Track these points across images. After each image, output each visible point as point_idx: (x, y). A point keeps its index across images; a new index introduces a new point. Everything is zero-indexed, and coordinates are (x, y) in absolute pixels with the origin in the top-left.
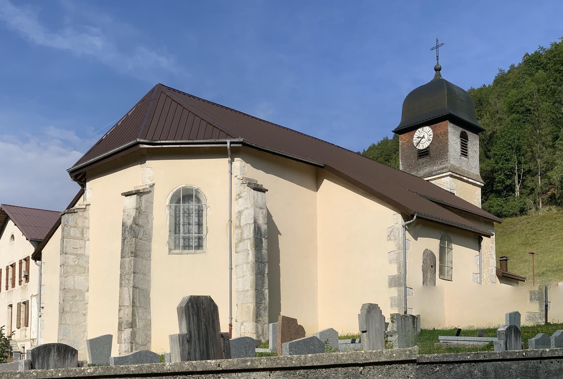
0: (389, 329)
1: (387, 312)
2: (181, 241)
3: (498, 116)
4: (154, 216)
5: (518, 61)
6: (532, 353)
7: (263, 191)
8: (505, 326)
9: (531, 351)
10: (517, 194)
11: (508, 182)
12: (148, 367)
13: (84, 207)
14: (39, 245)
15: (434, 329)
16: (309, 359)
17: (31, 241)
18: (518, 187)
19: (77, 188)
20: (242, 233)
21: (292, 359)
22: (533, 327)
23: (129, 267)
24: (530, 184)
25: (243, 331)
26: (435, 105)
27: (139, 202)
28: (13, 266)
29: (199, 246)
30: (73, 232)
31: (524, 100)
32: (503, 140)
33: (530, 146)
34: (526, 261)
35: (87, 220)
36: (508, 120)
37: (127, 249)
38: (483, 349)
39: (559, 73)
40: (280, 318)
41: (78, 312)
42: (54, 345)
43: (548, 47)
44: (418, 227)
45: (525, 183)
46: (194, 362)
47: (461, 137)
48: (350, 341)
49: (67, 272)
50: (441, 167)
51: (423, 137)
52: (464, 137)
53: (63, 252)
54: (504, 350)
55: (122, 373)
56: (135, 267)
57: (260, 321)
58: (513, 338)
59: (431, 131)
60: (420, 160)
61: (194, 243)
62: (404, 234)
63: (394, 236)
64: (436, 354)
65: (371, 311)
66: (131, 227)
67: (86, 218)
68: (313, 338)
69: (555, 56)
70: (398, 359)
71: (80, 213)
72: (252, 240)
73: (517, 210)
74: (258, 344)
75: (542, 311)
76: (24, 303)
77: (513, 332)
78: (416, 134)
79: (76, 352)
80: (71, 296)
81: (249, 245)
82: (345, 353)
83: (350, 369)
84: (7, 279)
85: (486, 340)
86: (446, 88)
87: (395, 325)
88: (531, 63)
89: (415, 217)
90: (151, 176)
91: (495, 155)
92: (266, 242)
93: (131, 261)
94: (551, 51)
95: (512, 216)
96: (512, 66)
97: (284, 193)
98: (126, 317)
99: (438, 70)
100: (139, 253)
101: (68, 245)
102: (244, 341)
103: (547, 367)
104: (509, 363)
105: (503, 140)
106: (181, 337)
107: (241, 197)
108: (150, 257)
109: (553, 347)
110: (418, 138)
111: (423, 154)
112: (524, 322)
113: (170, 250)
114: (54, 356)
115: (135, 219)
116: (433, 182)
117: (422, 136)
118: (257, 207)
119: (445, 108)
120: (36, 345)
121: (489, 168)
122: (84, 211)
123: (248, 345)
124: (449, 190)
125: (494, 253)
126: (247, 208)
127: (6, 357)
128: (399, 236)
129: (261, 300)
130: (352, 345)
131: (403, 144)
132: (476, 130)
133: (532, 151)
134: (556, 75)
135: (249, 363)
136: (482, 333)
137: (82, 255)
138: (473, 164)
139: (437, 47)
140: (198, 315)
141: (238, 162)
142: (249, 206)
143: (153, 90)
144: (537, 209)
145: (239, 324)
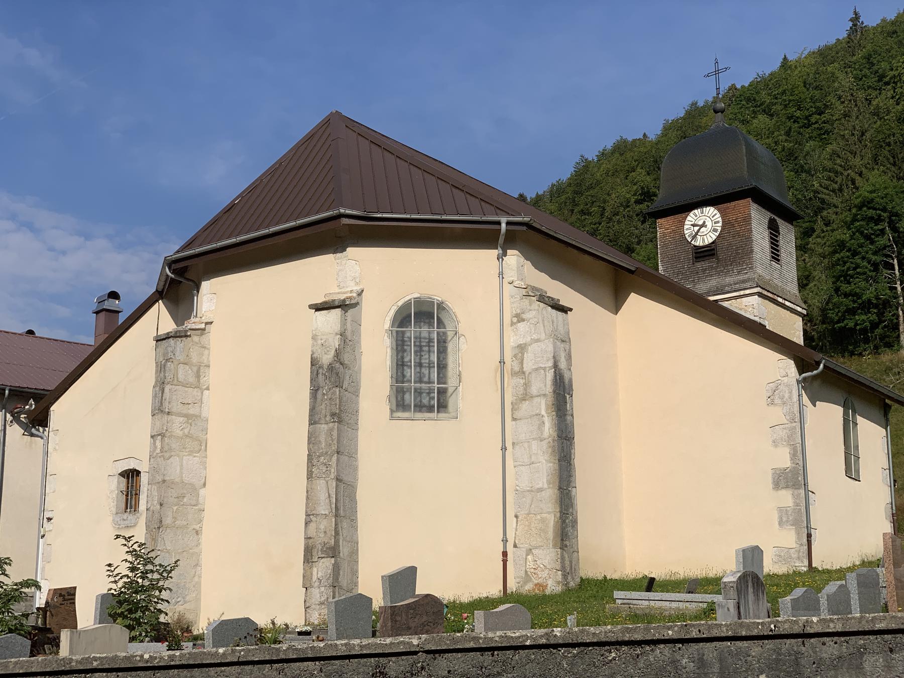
6: (786, 626)
7: (564, 310)
8: (735, 573)
9: (785, 622)
13: (203, 326)
15: (605, 577)
20: (527, 385)
22: (786, 576)
27: (344, 322)
29: (442, 406)
35: (206, 352)
37: (323, 408)
38: (697, 618)
39: (794, 122)
41: (186, 527)
47: (769, 228)
49: (170, 449)
50: (741, 277)
51: (704, 225)
52: (773, 228)
54: (736, 619)
57: (566, 546)
58: (751, 597)
59: (718, 215)
63: (782, 398)
64: (609, 627)
66: (331, 368)
67: (205, 348)
69: (784, 92)
71: (196, 338)
72: (550, 398)
75: (802, 545)
77: (750, 584)
78: (689, 218)
80: (175, 495)
81: (543, 407)
85: (703, 598)
86: (743, 142)
88: (744, 102)
89: (822, 366)
90: (357, 275)
93: (331, 430)
98: (322, 535)
101: (174, 397)
103: (815, 652)
104: (745, 644)
107: (523, 320)
109: (825, 615)
110: (694, 225)
111: (705, 253)
112: (770, 566)
113: (392, 411)
115: (338, 353)
116: (725, 304)
117: (700, 223)
122: (202, 335)
124: (757, 319)
126: (538, 341)
128: (790, 398)
131: (664, 235)
132: (790, 217)
134: (789, 124)
136: (693, 585)
137: (197, 416)
138: (786, 276)
139: (717, 72)
141: (513, 258)
142: (543, 336)
145: (521, 552)
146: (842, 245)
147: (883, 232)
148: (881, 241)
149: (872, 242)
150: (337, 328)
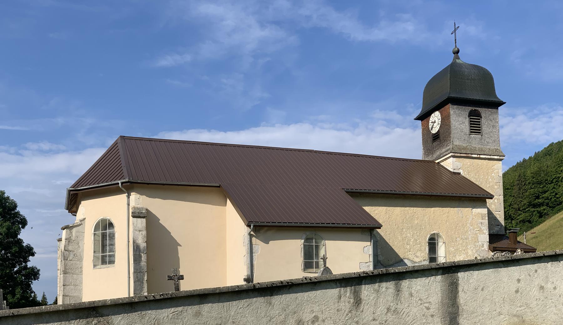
4: (85, 242)
99: (457, 52)
108: (81, 272)
110: (432, 122)
113: (95, 266)
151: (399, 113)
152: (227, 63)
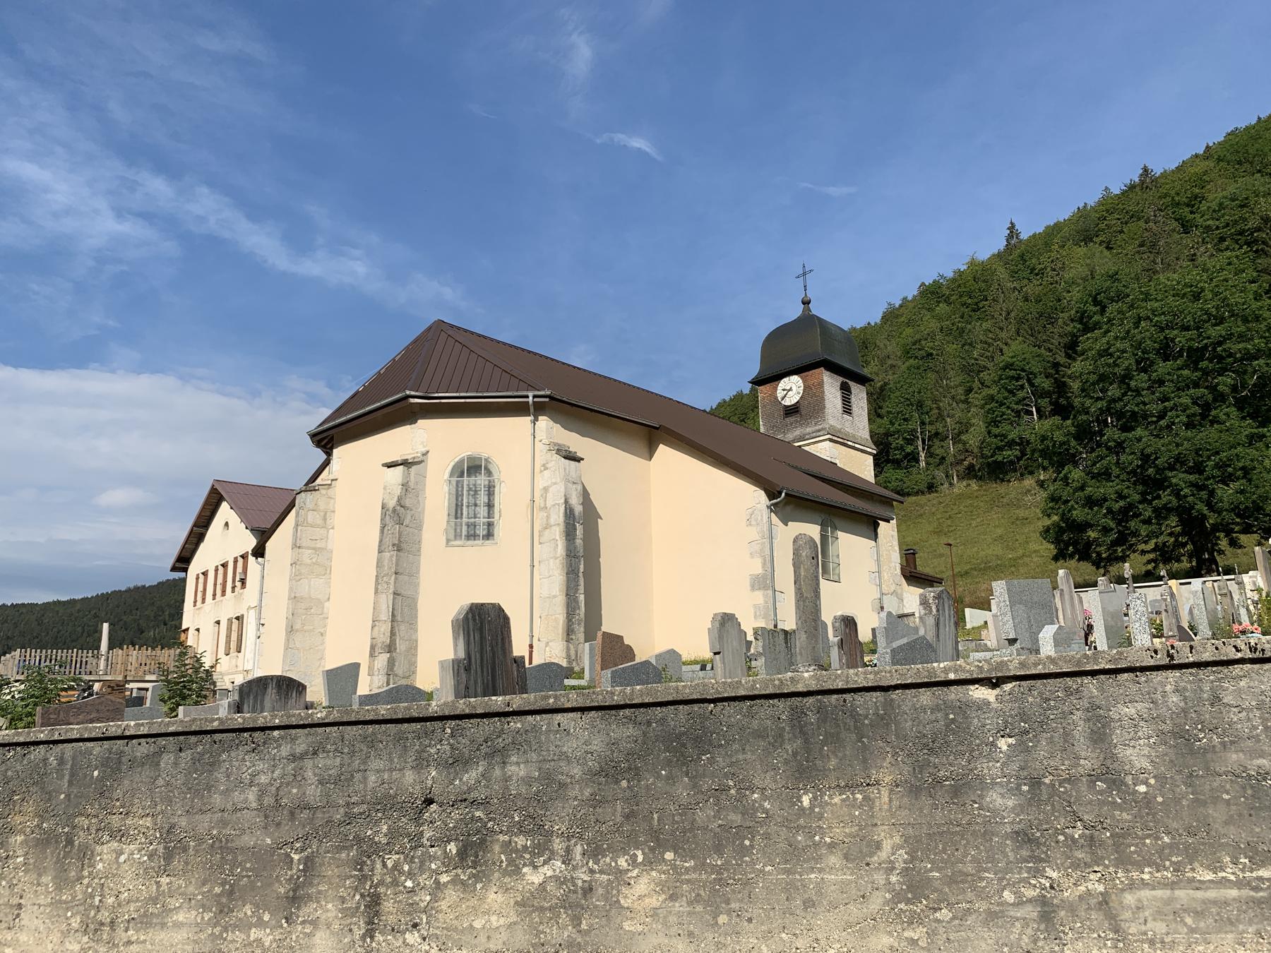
0: (752, 651)
1: (749, 624)
2: (464, 528)
3: (890, 362)
5: (912, 292)
7: (578, 460)
10: (923, 464)
11: (909, 449)
12: (405, 708)
14: (264, 536)
16: (638, 692)
17: (252, 530)
18: (922, 455)
19: (320, 456)
20: (548, 517)
21: (613, 693)
23: (388, 566)
24: (939, 451)
25: (548, 654)
26: (804, 347)
27: (407, 476)
28: (224, 565)
29: (489, 535)
30: (311, 517)
31: (923, 342)
32: (898, 394)
33: (935, 401)
34: (941, 555)
36: (904, 367)
40: (599, 634)
42: (272, 678)
43: (950, 274)
44: (788, 508)
45: (932, 450)
46: (472, 700)
48: (698, 667)
50: (817, 428)
51: (790, 389)
52: (845, 389)
53: (296, 546)
55: (368, 718)
56: (397, 565)
60: (787, 420)
61: (481, 531)
62: (770, 517)
65: (726, 622)
66: (394, 510)
68: (647, 663)
70: (763, 692)
71: (323, 492)
73: (923, 486)
74: (569, 673)
76: (237, 618)
79: (304, 687)
82: (434, 707)
83: (696, 707)
84: (215, 585)
87: (760, 643)
91: (889, 412)
92: (582, 532)
94: (953, 280)
95: (917, 493)
96: (905, 299)
97: (605, 461)
99: (806, 303)
100: (404, 546)
102: (548, 667)
105: (898, 394)
106: (456, 663)
108: (419, 550)
111: (792, 411)
113: (448, 541)
114: (271, 693)
115: (399, 499)
116: (806, 448)
118: (569, 481)
119: (817, 350)
120: (250, 677)
121: (882, 431)
123: (553, 674)
125: (896, 543)
127: (205, 697)
129: (574, 610)
130: (701, 674)
132: (862, 380)
133: (939, 408)
135: (551, 701)
138: (860, 424)
139: (804, 274)
140: (481, 630)
141: (544, 422)
143: (430, 328)
144: (951, 484)
145: (542, 645)
146: (992, 398)
147: (1022, 387)
148: (1021, 394)
149: (1014, 395)
150: (400, 480)
151: (330, 386)
152: (48, 258)
